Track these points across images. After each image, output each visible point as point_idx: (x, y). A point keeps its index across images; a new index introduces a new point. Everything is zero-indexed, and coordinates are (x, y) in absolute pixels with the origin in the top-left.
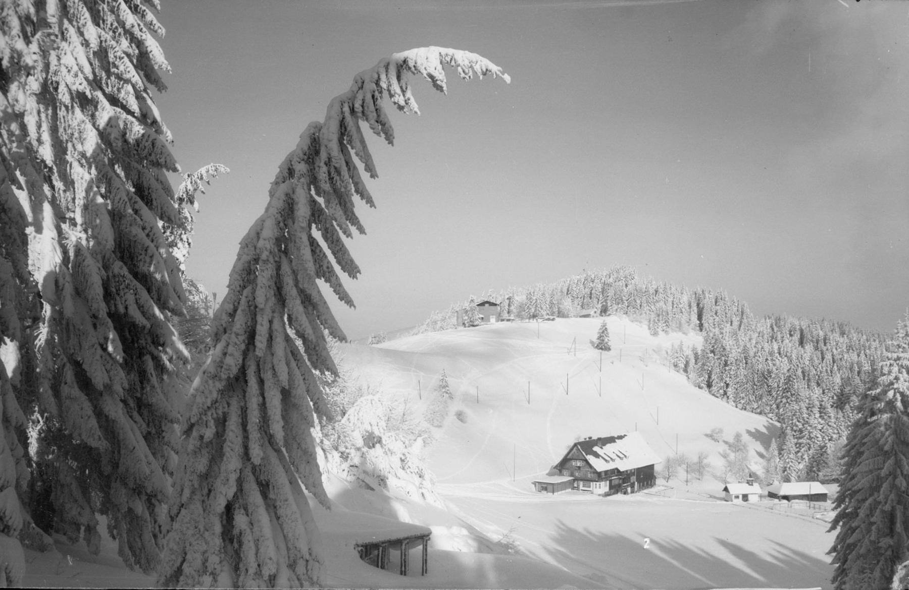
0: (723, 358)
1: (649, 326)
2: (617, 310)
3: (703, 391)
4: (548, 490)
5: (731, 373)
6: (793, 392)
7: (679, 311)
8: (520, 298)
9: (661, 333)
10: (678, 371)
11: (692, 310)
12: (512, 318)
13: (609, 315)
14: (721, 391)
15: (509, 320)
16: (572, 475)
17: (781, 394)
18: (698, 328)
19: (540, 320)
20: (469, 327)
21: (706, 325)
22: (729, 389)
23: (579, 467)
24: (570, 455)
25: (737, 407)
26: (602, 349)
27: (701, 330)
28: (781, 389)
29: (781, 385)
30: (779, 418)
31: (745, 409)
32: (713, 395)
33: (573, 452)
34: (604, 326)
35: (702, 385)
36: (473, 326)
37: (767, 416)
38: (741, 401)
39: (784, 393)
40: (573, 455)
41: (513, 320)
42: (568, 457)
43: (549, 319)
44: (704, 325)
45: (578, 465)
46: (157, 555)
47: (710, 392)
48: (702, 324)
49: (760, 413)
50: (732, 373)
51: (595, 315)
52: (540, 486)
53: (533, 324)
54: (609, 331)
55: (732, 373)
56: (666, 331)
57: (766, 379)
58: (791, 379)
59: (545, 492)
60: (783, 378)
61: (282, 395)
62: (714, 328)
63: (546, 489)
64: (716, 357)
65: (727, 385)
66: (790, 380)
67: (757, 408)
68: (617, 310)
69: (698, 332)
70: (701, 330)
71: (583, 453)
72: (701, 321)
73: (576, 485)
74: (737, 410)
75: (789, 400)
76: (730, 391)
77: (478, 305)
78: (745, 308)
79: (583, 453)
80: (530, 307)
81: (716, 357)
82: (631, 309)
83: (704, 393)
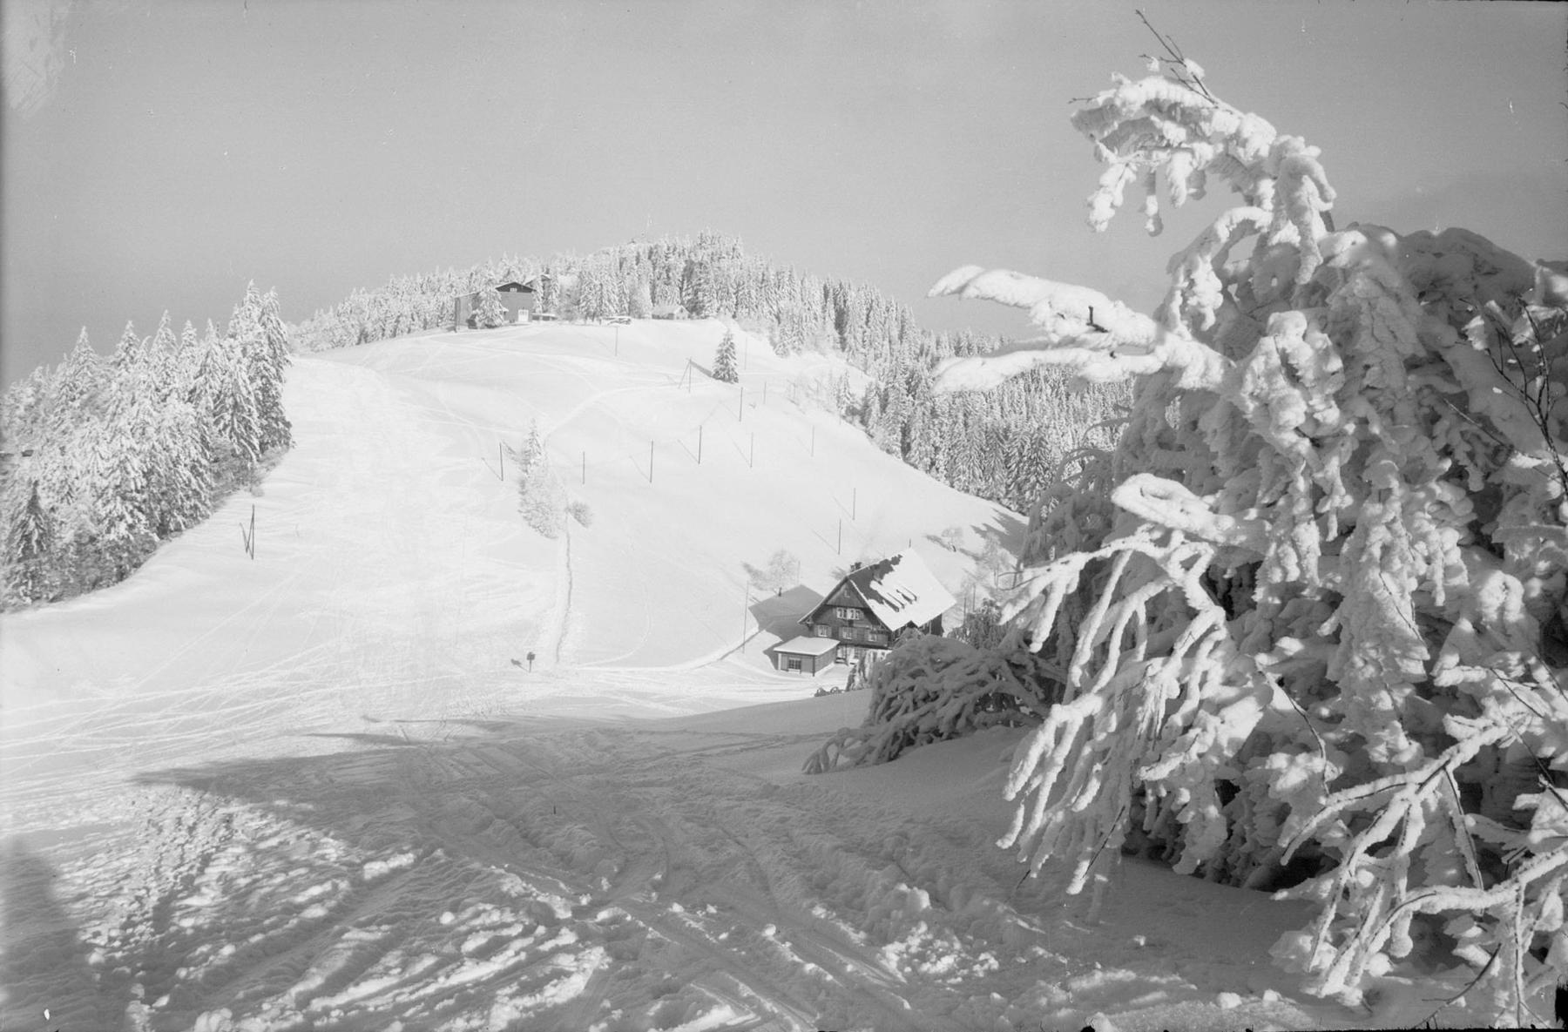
0: (928, 404)
1: (771, 339)
2: (719, 309)
3: (893, 457)
4: (803, 667)
5: (943, 429)
6: (1046, 465)
7: (812, 316)
8: (566, 281)
9: (792, 353)
10: (851, 422)
11: (827, 314)
12: (553, 315)
13: (706, 317)
14: (927, 460)
15: (546, 319)
16: (834, 636)
17: (1026, 468)
18: (839, 345)
19: (605, 322)
20: (482, 328)
21: (850, 341)
22: (940, 456)
23: (851, 622)
24: (834, 598)
25: (952, 486)
26: (723, 379)
27: (843, 349)
28: (1025, 459)
29: (1025, 453)
30: (1021, 506)
31: (967, 491)
32: (912, 465)
33: (838, 593)
34: (729, 339)
35: (894, 447)
36: (490, 327)
37: (1001, 503)
38: (961, 477)
39: (1031, 465)
40: (839, 598)
41: (553, 318)
42: (829, 603)
43: (620, 321)
44: (848, 340)
45: (849, 617)
46: (461, 1016)
47: (906, 460)
48: (845, 340)
49: (989, 498)
50: (944, 428)
51: (681, 316)
52: (786, 659)
53: (594, 329)
54: (736, 348)
55: (944, 428)
56: (799, 349)
57: (1001, 441)
58: (1044, 443)
59: (797, 672)
60: (1029, 441)
61: (1450, 736)
62: (864, 347)
63: (798, 666)
64: (917, 402)
65: (937, 449)
66: (1041, 445)
67: (986, 489)
68: (719, 309)
69: (840, 351)
70: (843, 349)
71: (862, 595)
72: (841, 333)
73: (840, 655)
74: (954, 491)
75: (1040, 479)
76: (942, 459)
77: (498, 289)
78: (907, 316)
79: (862, 595)
80: (590, 297)
81: (917, 402)
82: (743, 311)
83: (896, 461)
